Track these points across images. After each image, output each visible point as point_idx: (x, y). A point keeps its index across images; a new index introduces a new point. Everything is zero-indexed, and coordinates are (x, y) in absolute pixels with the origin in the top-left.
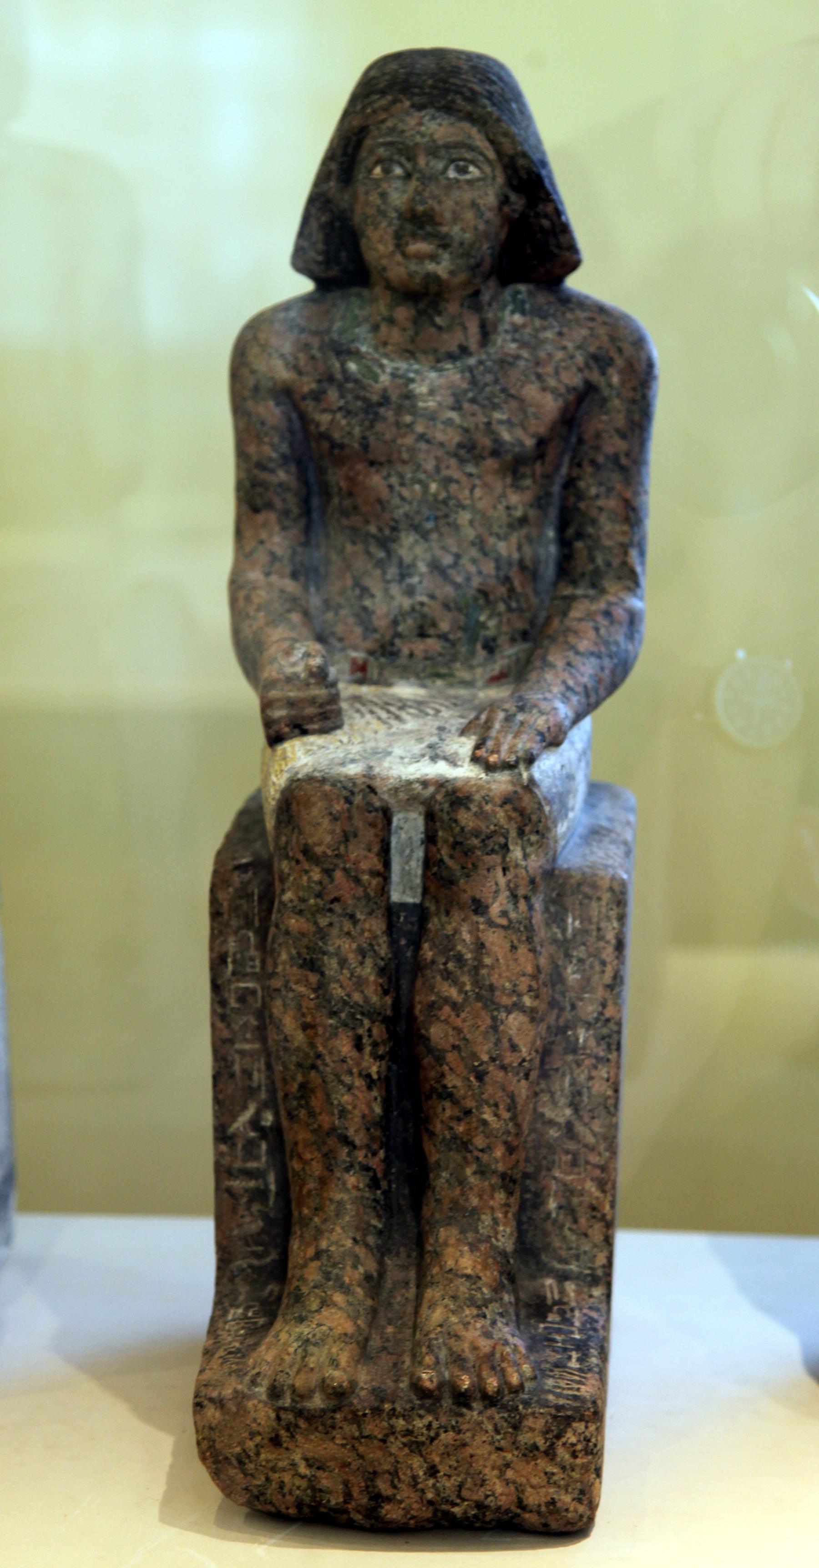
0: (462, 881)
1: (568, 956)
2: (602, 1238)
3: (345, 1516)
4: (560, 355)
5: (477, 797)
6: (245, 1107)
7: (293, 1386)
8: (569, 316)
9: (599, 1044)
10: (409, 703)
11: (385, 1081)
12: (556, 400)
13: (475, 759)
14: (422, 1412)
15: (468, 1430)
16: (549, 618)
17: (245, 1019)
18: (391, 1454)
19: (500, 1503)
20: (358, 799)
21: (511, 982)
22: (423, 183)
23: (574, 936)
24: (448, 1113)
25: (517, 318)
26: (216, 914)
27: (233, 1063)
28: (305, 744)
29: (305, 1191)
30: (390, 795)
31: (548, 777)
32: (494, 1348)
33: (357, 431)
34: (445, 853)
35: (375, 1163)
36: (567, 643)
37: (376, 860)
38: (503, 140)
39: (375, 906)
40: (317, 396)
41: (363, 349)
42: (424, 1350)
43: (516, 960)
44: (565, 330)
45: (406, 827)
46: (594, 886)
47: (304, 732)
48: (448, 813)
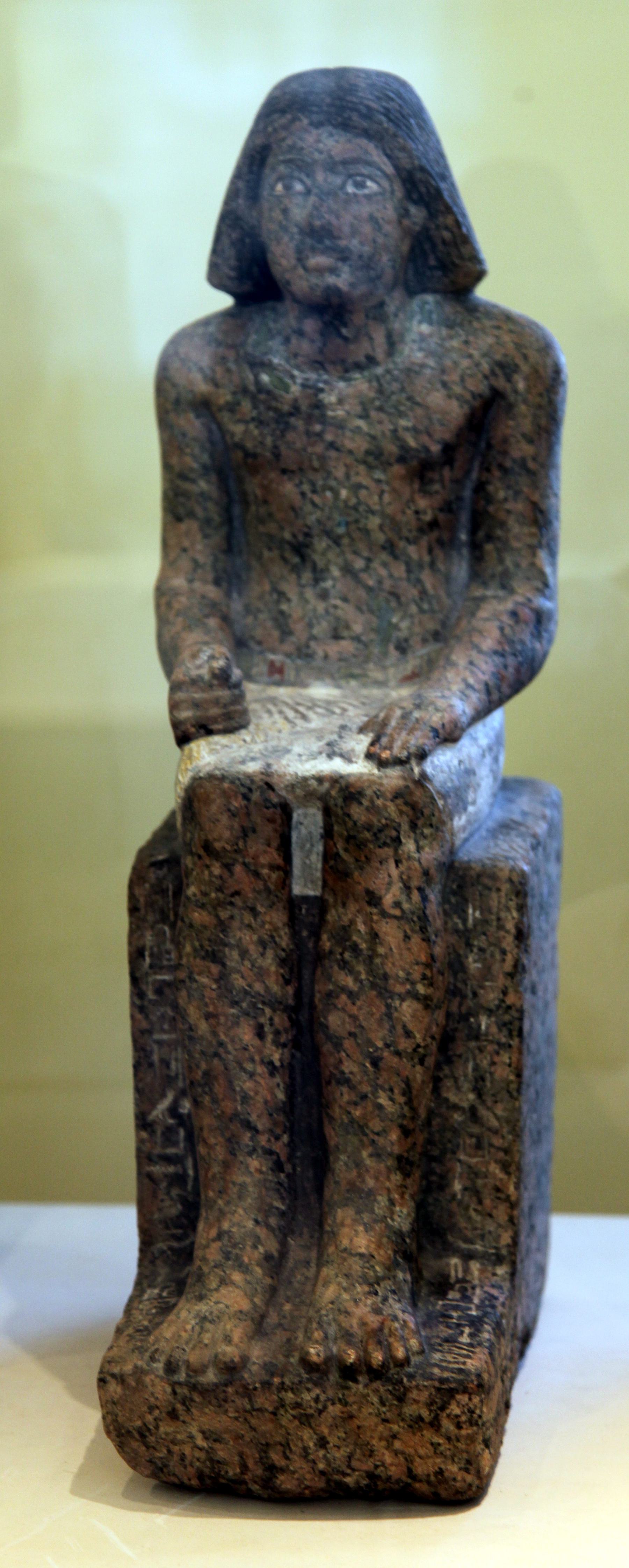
0: (356, 874)
1: (469, 945)
2: (506, 1218)
3: (244, 1487)
4: (465, 363)
5: (369, 792)
6: (163, 1096)
7: (188, 1361)
8: (476, 324)
9: (500, 1030)
10: (319, 703)
11: (289, 1068)
12: (461, 407)
13: (369, 756)
14: (310, 1386)
15: (354, 1403)
16: (459, 618)
17: (162, 1010)
18: (281, 1426)
19: (389, 1473)
20: (255, 796)
21: (404, 970)
22: (321, 199)
23: (475, 926)
24: (346, 1098)
25: (425, 328)
26: (133, 910)
27: (152, 1052)
28: (209, 744)
29: (210, 1175)
30: (287, 791)
31: (442, 772)
32: (382, 1323)
33: (269, 441)
34: (340, 845)
35: (280, 1147)
36: (471, 642)
37: (275, 854)
38: (401, 155)
39: (275, 899)
40: (232, 408)
41: (276, 361)
42: (315, 1325)
43: (409, 949)
44: (471, 339)
45: (306, 822)
46: (494, 877)
47: (209, 732)
48: (342, 808)
